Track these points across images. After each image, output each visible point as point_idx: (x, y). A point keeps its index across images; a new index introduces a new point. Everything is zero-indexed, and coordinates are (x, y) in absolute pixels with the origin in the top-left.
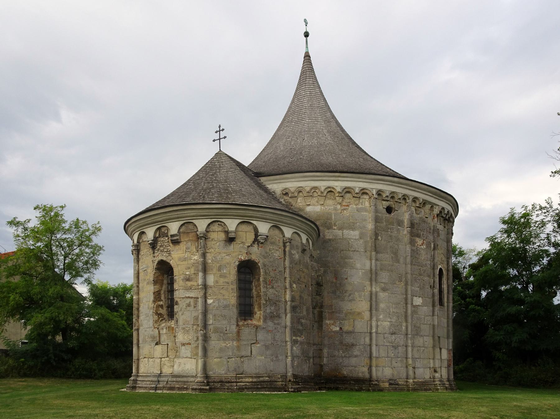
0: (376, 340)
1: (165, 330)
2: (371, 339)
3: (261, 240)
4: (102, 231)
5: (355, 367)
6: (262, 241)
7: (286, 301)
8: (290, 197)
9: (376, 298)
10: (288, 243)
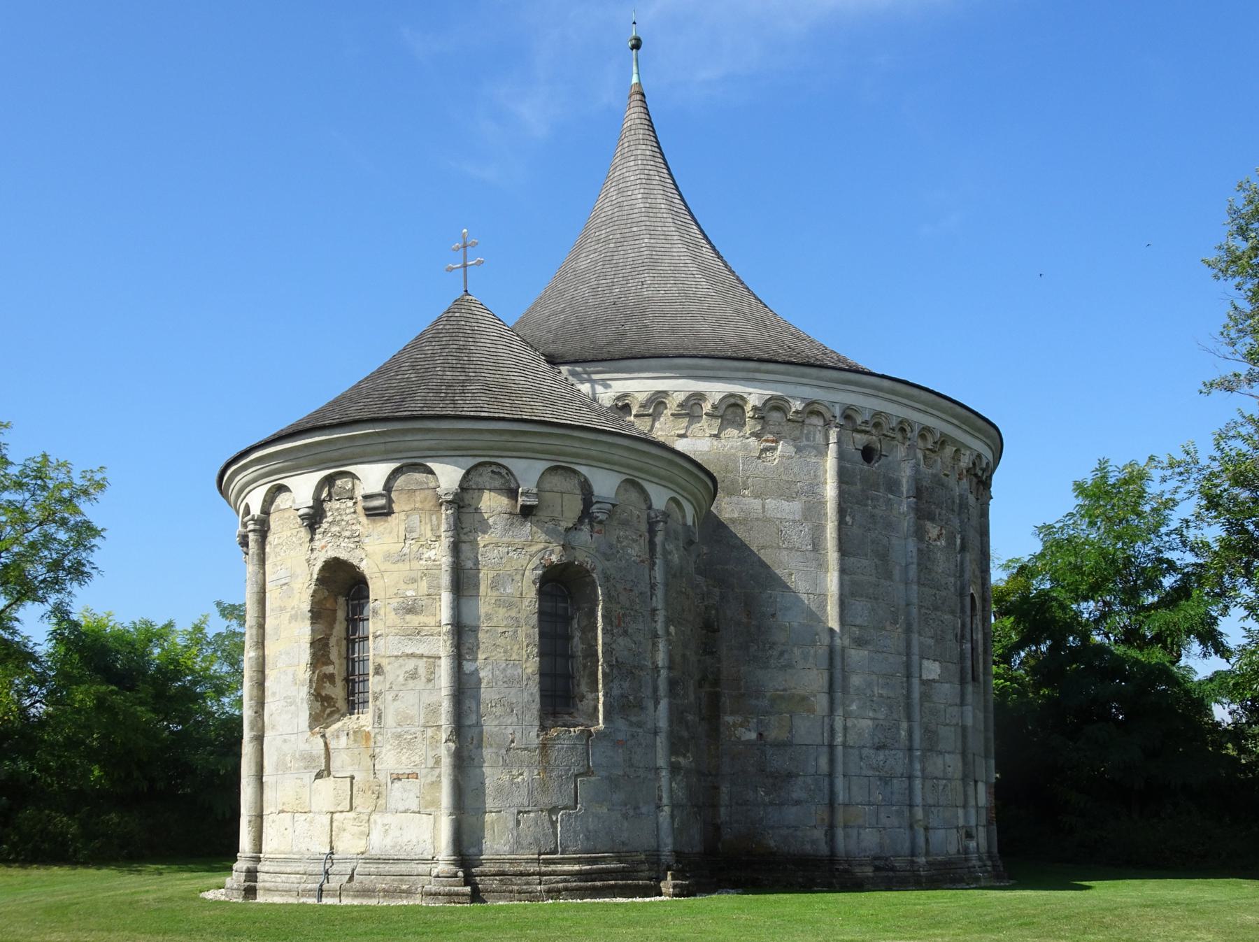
0: (844, 763)
1: (344, 739)
2: (832, 761)
3: (598, 515)
4: (109, 490)
5: (796, 828)
6: (602, 517)
7: (657, 667)
8: (636, 416)
9: (843, 659)
10: (662, 523)
